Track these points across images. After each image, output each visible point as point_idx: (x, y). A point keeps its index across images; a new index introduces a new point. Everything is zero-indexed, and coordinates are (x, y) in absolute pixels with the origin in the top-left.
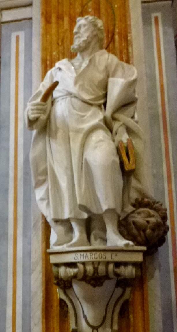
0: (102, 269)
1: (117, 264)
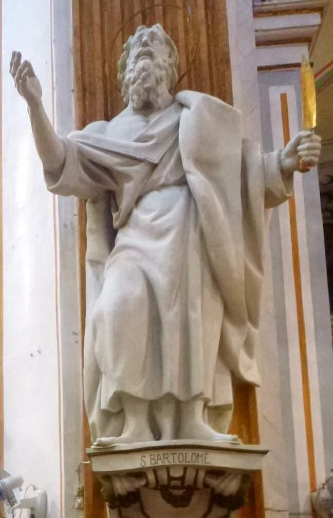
0: (190, 475)
1: (218, 473)
